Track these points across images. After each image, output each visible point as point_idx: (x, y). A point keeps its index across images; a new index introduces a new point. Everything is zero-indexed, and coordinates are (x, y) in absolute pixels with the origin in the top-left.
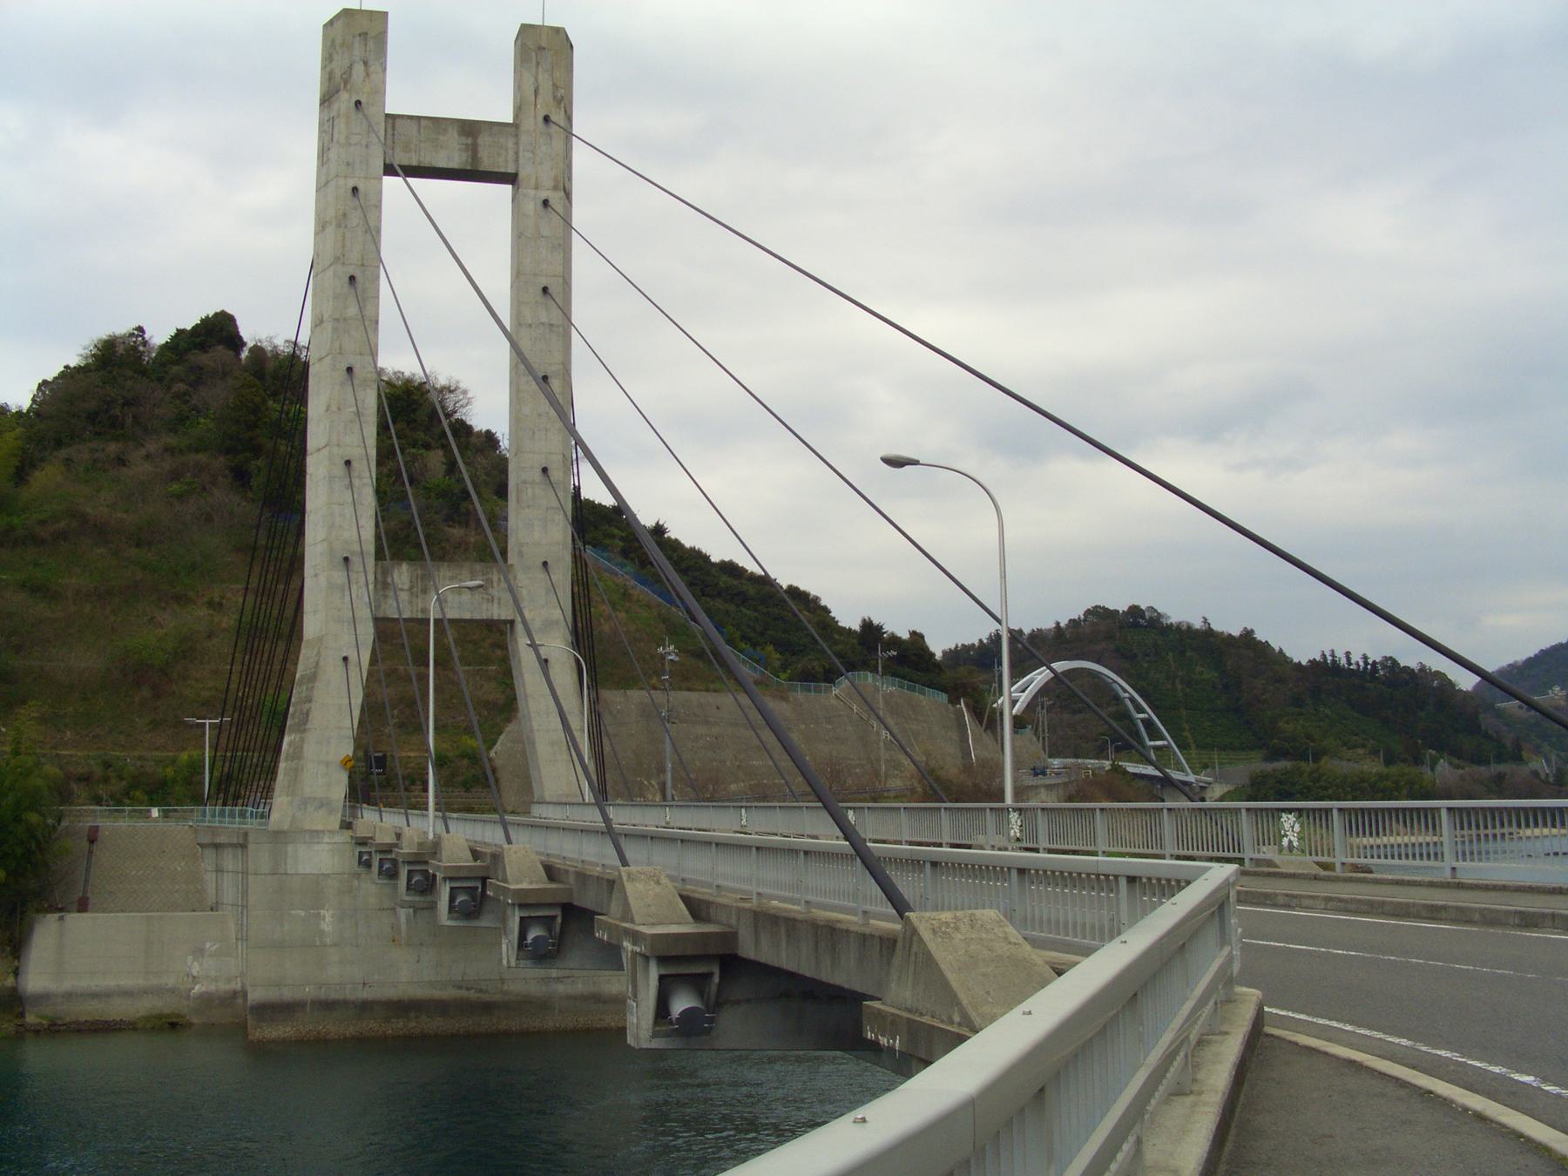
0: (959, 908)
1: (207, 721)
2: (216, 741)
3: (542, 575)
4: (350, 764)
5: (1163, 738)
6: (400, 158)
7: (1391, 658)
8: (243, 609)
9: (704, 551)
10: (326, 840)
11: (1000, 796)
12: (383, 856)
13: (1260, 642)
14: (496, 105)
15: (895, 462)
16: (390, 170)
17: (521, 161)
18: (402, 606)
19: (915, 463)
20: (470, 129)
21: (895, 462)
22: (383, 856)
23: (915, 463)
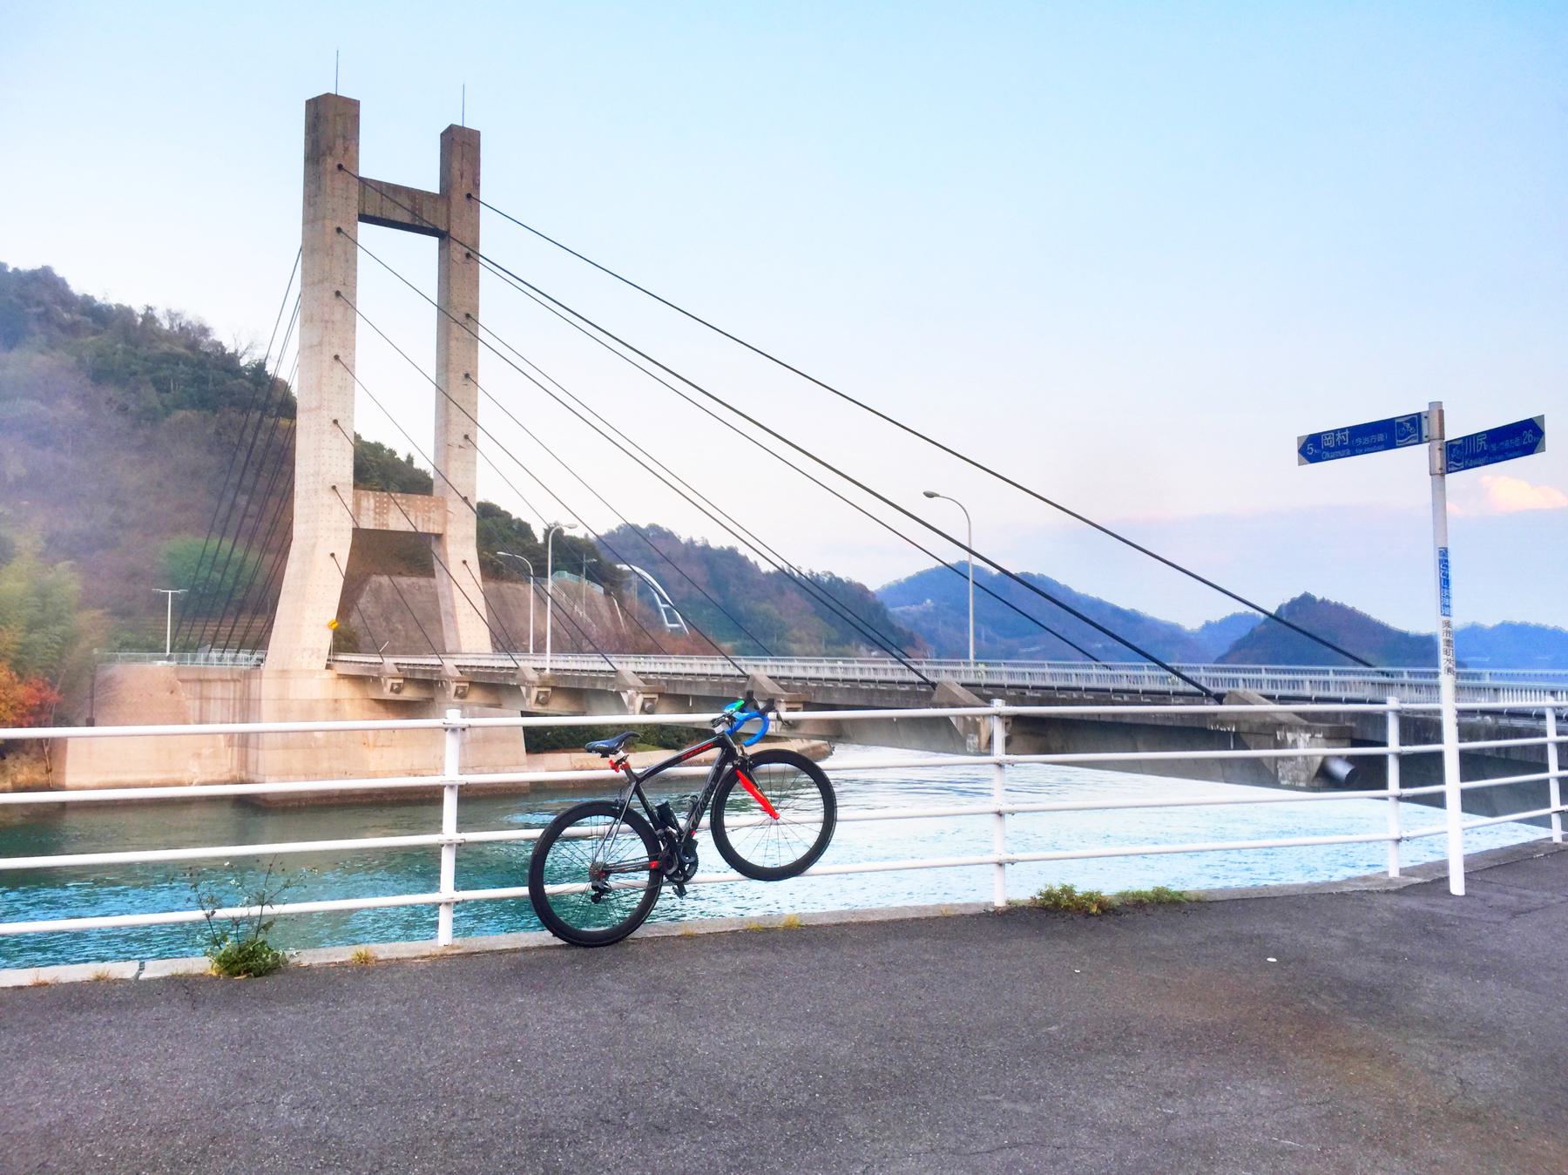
0: (1266, 682)
1: (170, 592)
2: (732, 622)
3: (333, 496)
4: (334, 626)
5: (678, 622)
6: (369, 212)
7: (830, 573)
8: (217, 511)
9: (1339, 602)
10: (317, 677)
11: (968, 657)
12: (458, 685)
13: (742, 556)
14: (428, 180)
15: (930, 495)
16: (364, 218)
17: (452, 224)
18: (368, 523)
19: (938, 496)
20: (412, 194)
21: (930, 495)
22: (458, 685)
23: (938, 496)
